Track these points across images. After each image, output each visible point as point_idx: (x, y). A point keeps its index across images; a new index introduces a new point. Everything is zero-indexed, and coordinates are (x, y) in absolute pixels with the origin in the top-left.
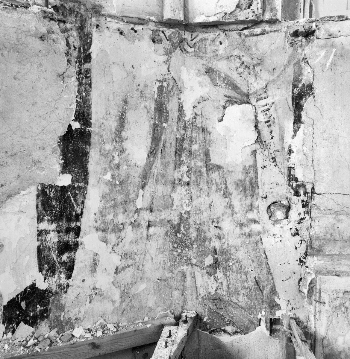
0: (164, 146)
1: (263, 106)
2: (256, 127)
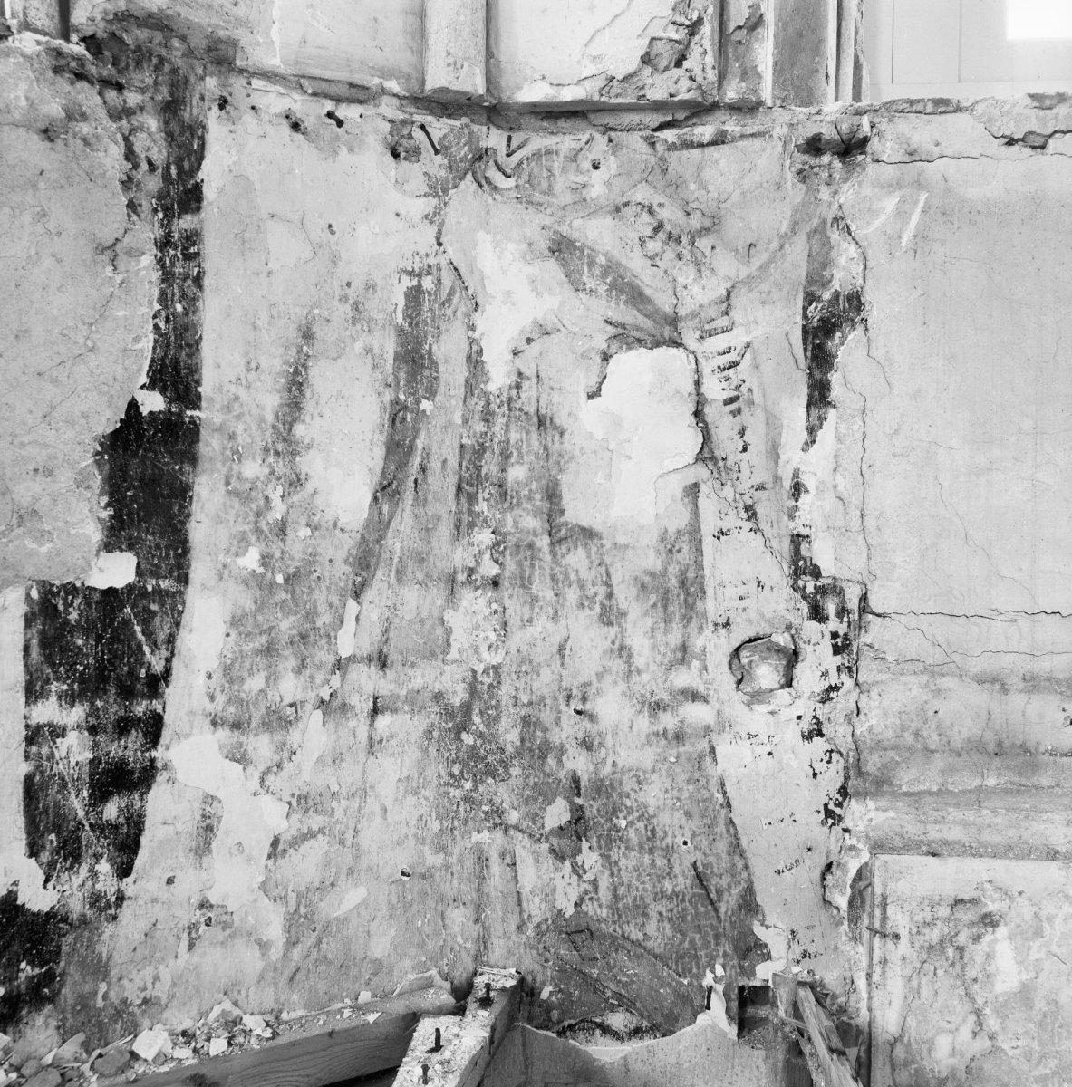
0: (423, 469)
2: (698, 414)
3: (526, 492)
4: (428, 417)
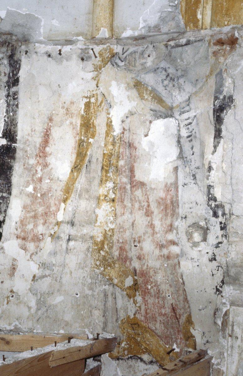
0: (90, 162)
1: (186, 120)
2: (179, 142)
3: (124, 169)
4: (91, 144)
